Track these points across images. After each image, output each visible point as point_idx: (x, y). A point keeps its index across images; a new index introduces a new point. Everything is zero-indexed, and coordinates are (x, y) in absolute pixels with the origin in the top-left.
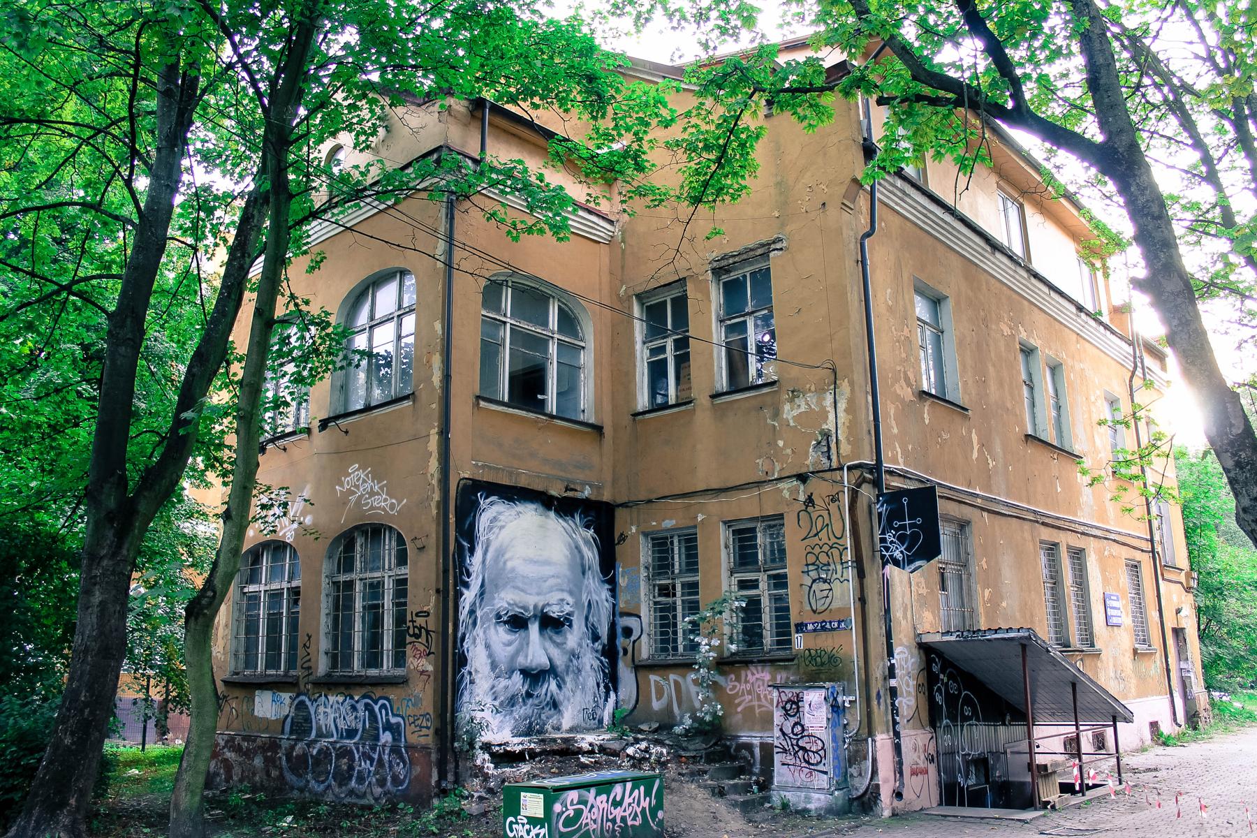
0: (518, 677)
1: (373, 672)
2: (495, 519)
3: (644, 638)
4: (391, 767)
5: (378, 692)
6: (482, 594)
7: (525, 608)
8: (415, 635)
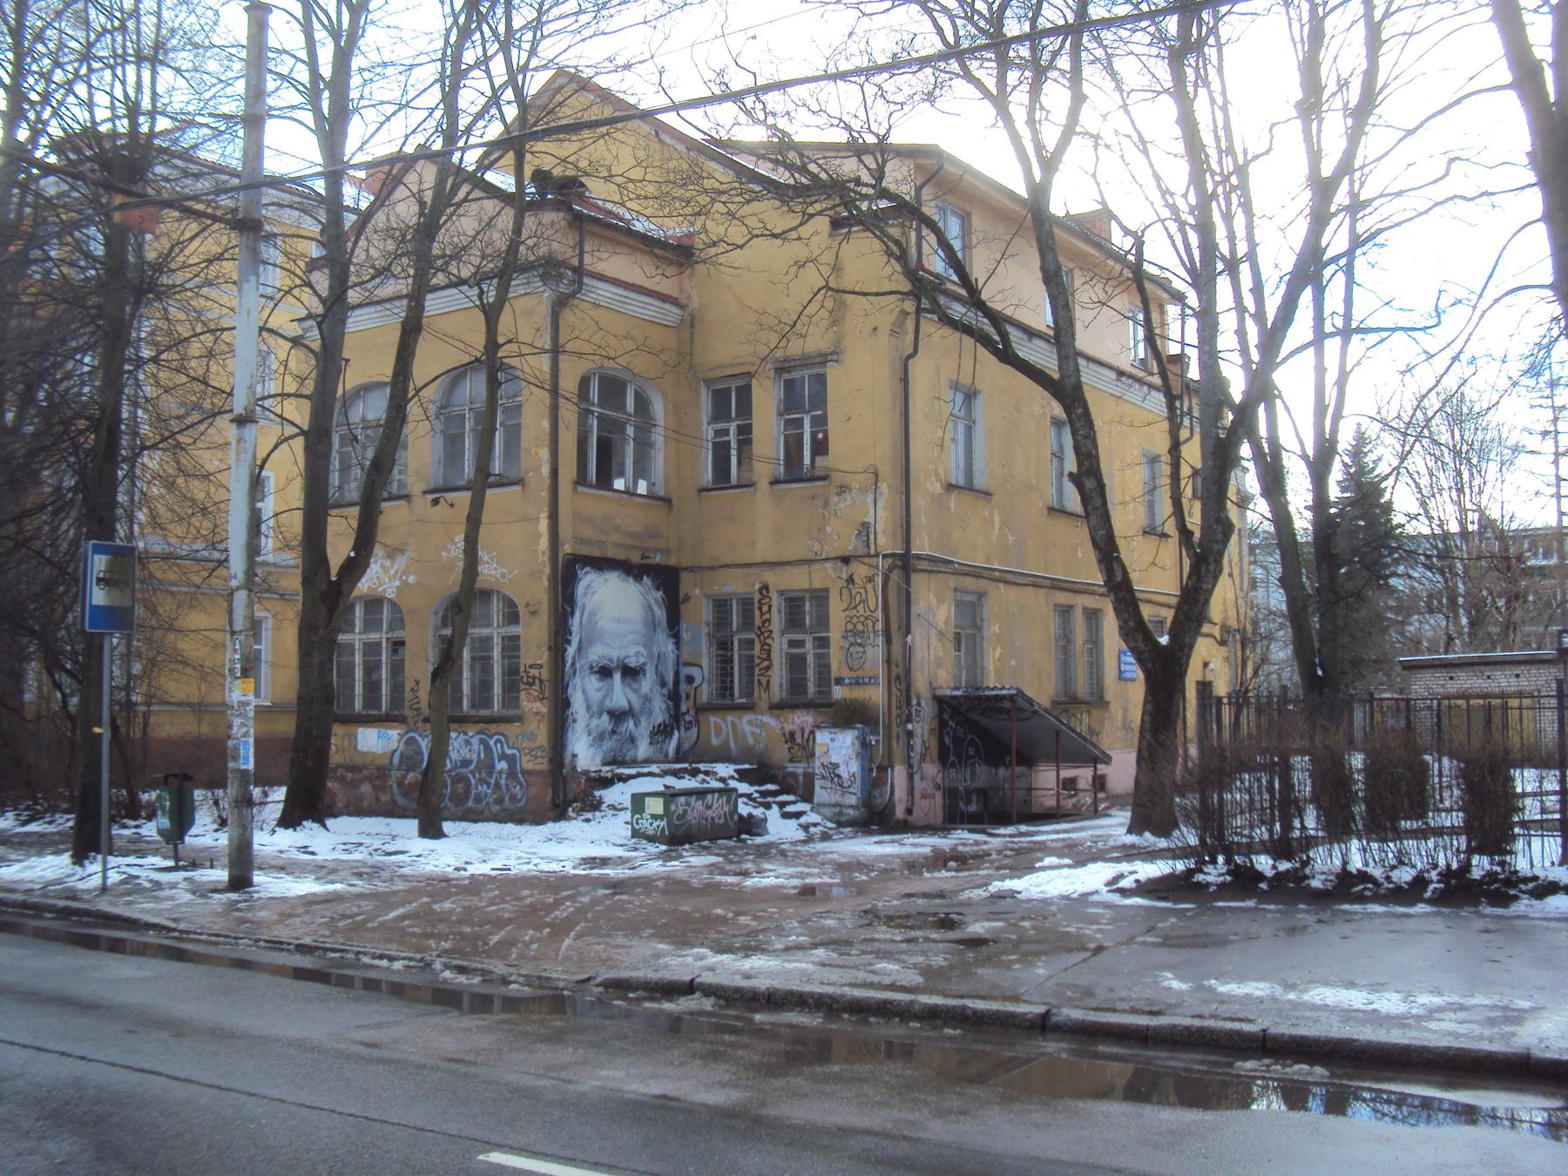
0: (605, 718)
1: (483, 712)
2: (588, 587)
3: (705, 686)
4: (508, 789)
5: (493, 728)
6: (580, 649)
7: (611, 660)
8: (528, 683)
